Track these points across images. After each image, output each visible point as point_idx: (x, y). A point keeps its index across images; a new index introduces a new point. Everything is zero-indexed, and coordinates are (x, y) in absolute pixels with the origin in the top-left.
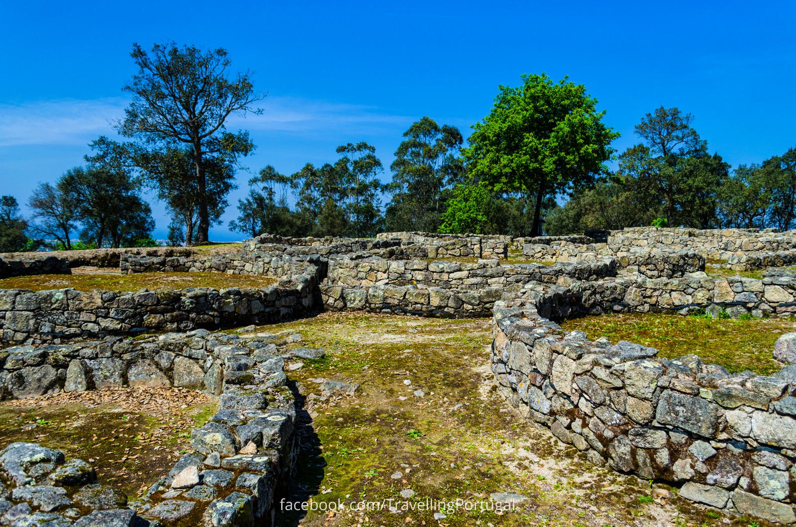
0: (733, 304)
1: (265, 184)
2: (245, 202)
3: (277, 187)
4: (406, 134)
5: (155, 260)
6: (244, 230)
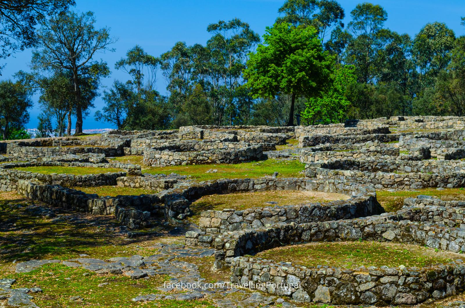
0: (223, 149)
1: (133, 67)
2: (110, 93)
3: (145, 69)
4: (281, 10)
5: (69, 141)
6: (109, 120)
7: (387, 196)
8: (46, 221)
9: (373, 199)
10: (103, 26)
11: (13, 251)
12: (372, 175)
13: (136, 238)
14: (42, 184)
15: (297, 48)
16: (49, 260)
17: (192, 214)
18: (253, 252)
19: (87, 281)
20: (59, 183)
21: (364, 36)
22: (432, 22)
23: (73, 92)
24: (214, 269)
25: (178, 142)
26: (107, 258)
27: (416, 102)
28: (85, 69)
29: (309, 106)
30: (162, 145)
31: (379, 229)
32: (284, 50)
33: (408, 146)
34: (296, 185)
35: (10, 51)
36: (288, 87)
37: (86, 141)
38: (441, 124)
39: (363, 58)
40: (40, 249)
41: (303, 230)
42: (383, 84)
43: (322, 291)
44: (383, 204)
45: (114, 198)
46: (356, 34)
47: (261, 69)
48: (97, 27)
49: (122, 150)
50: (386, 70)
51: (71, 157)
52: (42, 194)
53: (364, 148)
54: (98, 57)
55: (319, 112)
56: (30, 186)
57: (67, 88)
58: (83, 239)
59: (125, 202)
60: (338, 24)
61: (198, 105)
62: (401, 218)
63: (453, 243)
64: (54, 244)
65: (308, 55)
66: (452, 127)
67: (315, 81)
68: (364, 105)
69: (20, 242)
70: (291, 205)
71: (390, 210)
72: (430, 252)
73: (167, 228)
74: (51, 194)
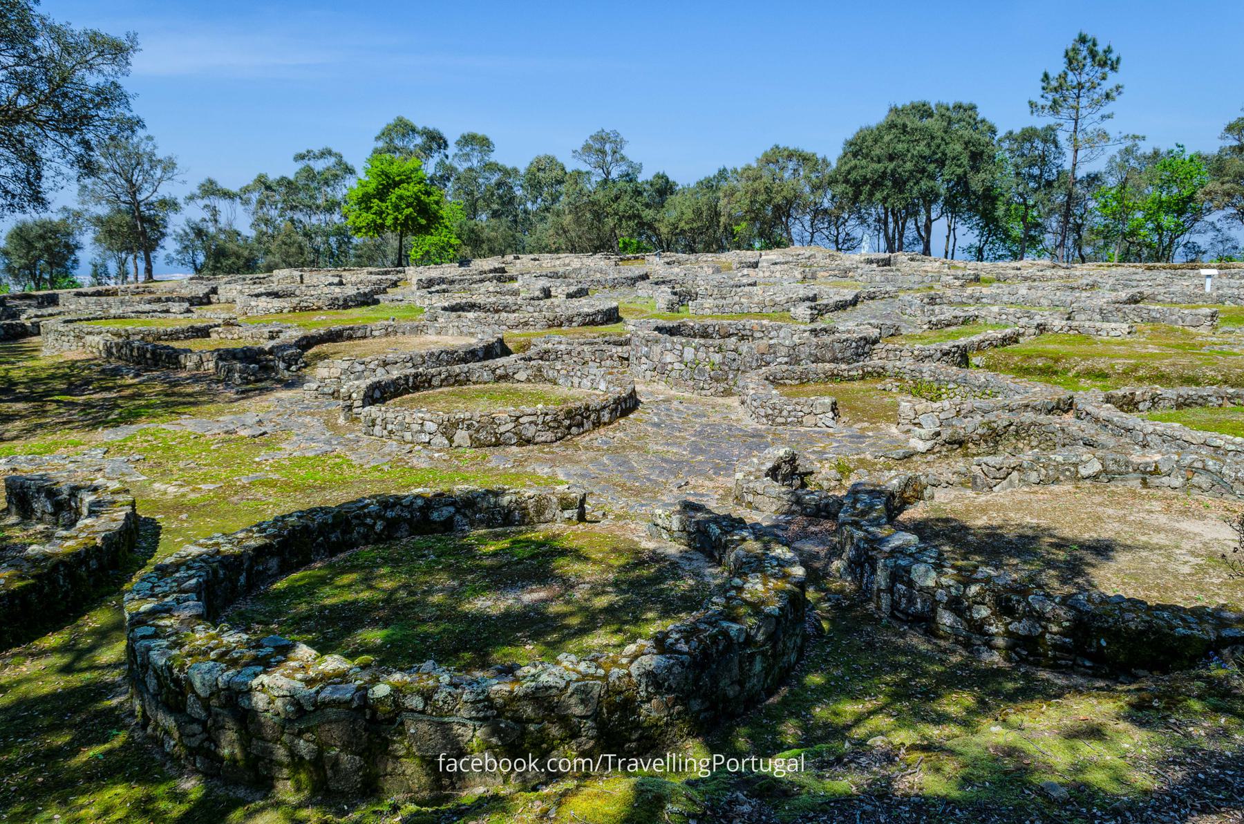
1: (206, 202)
3: (222, 205)
4: (378, 138)
7: (513, 338)
8: (131, 381)
9: (501, 341)
10: (168, 154)
11: (94, 418)
12: (496, 316)
13: (244, 394)
14: (116, 340)
15: (402, 182)
16: (143, 424)
17: (307, 365)
18: (383, 400)
19: (197, 444)
20: (139, 337)
21: (471, 169)
22: (542, 154)
23: (137, 232)
24: (341, 421)
25: (275, 287)
26: (216, 418)
27: (529, 240)
28: (150, 205)
29: (417, 245)
30: (257, 291)
31: (510, 371)
32: (387, 185)
33: (527, 285)
34: (418, 330)
35: (64, 183)
36: (395, 224)
37: (160, 289)
38: (558, 262)
39: (471, 193)
40: (130, 412)
41: (433, 376)
42: (494, 222)
43: (461, 436)
44: (510, 346)
45: (212, 352)
46: (461, 167)
47: (363, 205)
48: (160, 155)
49: (209, 298)
50: (495, 207)
51: (147, 307)
52: (118, 351)
53: (483, 290)
54: (165, 191)
55: (428, 252)
56: (102, 342)
57: (129, 228)
58: (181, 399)
59: (226, 355)
60: (442, 156)
61: (290, 245)
62: (530, 359)
63: (585, 381)
64: (147, 406)
65: (416, 189)
66: (568, 265)
67: (424, 217)
68: (476, 243)
69: (102, 407)
70: (417, 351)
71: (518, 351)
72: (563, 390)
73: (279, 381)
74: (132, 351)
